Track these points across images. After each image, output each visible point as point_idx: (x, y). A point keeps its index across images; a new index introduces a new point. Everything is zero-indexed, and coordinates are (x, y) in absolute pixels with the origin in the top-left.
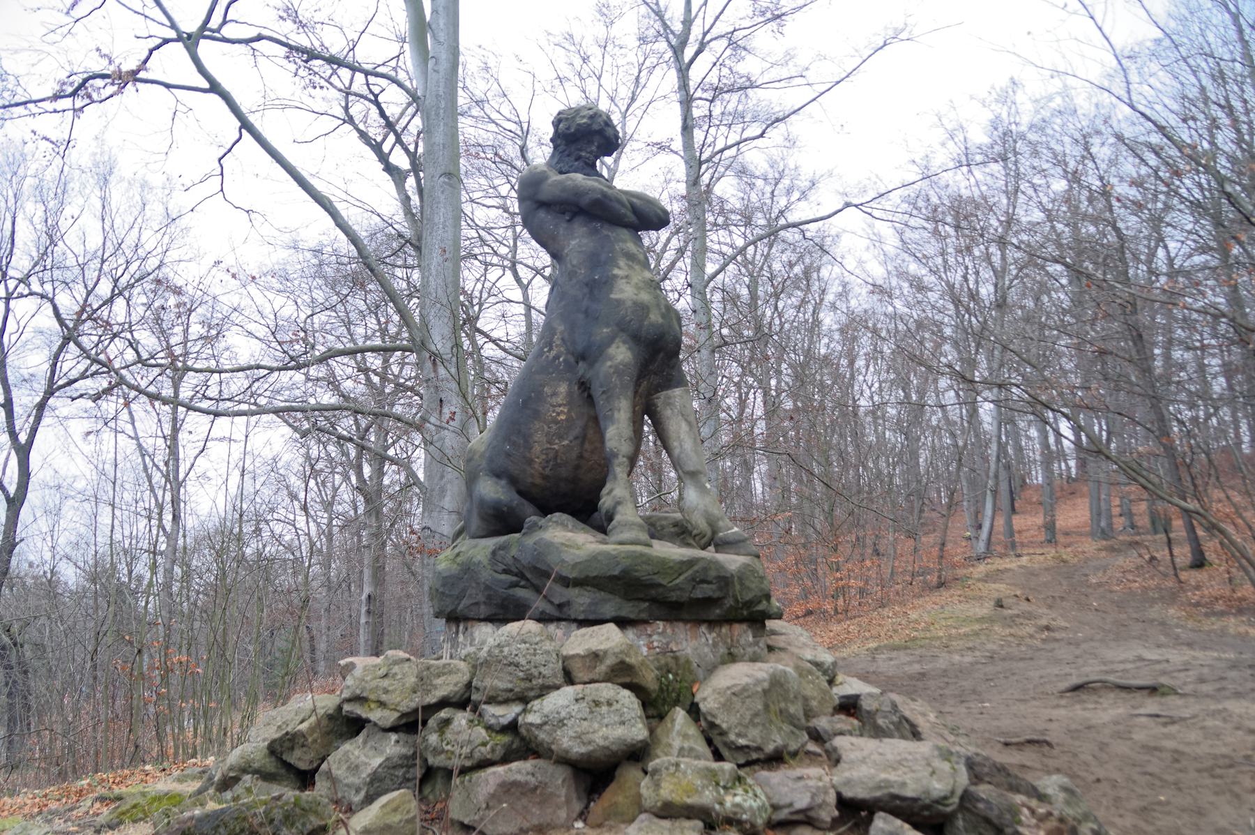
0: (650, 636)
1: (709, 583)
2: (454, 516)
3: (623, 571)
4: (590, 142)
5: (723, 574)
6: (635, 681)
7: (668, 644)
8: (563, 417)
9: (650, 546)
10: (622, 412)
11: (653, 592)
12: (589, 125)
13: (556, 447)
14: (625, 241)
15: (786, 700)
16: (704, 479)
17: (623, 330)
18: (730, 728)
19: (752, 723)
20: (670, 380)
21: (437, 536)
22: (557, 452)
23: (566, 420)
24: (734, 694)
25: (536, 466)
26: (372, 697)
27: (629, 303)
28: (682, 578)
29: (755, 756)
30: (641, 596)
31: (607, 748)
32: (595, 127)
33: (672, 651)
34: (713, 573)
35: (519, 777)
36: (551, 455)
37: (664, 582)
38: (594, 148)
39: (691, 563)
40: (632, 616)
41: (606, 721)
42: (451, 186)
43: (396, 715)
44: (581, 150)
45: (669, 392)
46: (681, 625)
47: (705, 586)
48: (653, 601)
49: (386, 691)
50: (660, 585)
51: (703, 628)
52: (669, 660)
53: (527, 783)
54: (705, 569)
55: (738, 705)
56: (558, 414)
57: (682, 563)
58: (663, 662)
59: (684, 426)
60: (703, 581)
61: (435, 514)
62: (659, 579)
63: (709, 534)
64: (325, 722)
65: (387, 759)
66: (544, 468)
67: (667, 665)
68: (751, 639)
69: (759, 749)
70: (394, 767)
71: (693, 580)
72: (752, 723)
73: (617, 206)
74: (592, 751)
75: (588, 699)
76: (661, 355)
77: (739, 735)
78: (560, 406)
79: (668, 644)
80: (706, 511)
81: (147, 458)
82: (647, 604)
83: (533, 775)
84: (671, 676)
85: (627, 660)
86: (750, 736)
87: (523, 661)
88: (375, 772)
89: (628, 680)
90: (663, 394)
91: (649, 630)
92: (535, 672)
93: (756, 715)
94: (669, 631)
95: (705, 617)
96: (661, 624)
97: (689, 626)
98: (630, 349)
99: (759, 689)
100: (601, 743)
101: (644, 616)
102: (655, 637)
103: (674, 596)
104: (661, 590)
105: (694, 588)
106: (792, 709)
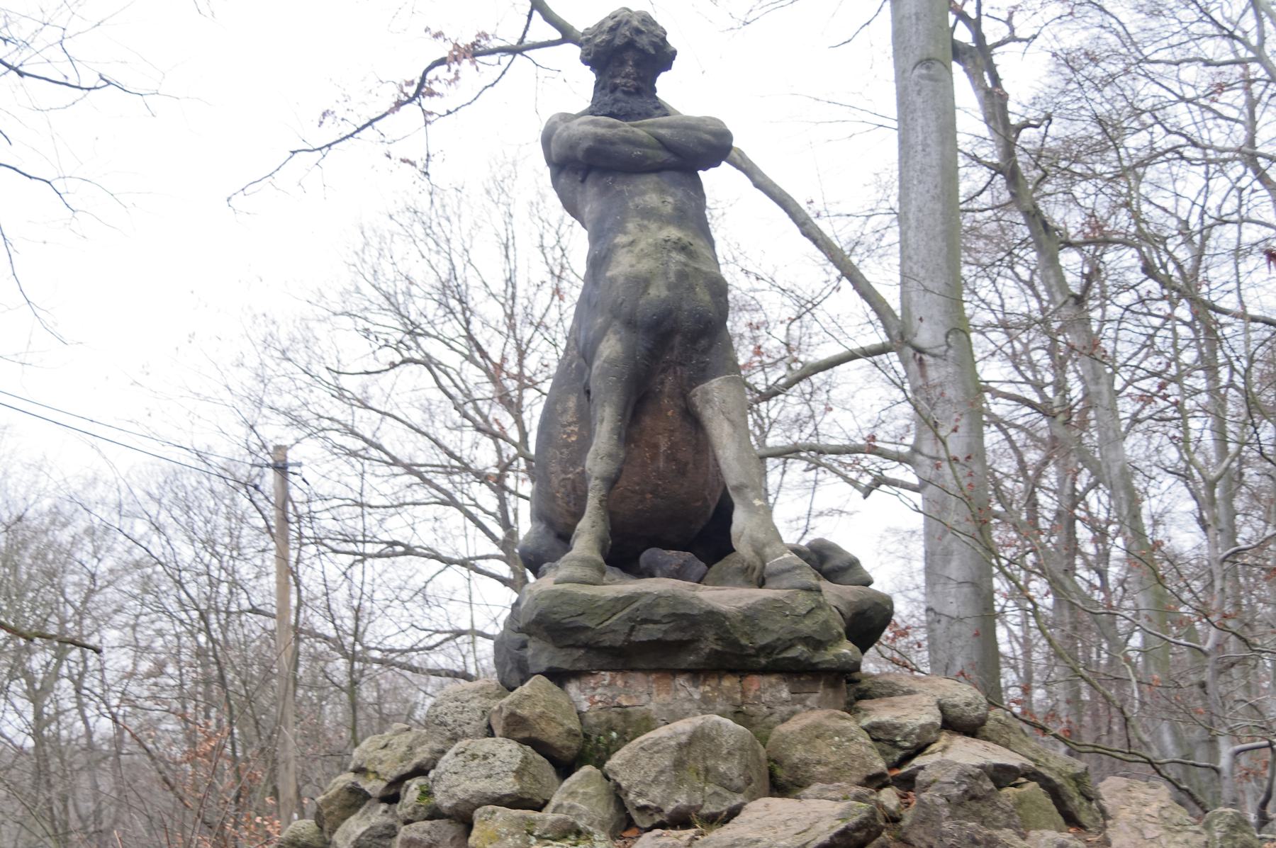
0: (594, 689)
1: (656, 622)
2: (966, 589)
3: (539, 615)
4: (623, 63)
5: (682, 610)
6: (533, 735)
7: (613, 698)
8: (574, 438)
9: (819, 591)
10: (605, 424)
11: (582, 637)
12: (609, 42)
13: (570, 476)
14: (643, 193)
15: (716, 755)
16: (751, 495)
17: (615, 317)
18: (630, 787)
19: (655, 781)
20: (704, 370)
21: (944, 620)
22: (573, 481)
23: (577, 442)
24: (642, 748)
25: (560, 502)
26: (370, 768)
27: (621, 280)
28: (615, 618)
29: (658, 818)
30: (571, 642)
31: (467, 801)
32: (618, 41)
33: (620, 706)
34: (663, 611)
35: (416, 835)
36: (569, 487)
37: (591, 624)
38: (629, 69)
39: (630, 599)
40: (566, 666)
41: (472, 774)
42: (931, 78)
43: (384, 784)
44: (614, 77)
45: (706, 385)
46: (639, 676)
47: (650, 626)
48: (587, 646)
49: (381, 762)
50: (587, 628)
51: (681, 681)
52: (614, 715)
53: (421, 841)
54: (649, 607)
55: (644, 762)
56: (569, 436)
57: (617, 600)
58: (603, 719)
59: (727, 428)
60: (645, 621)
61: (939, 588)
62: (582, 621)
63: (758, 564)
64: (345, 795)
65: (372, 828)
66: (568, 503)
67: (609, 721)
68: (785, 694)
69: (659, 810)
70: (380, 837)
71: (630, 619)
72: (655, 781)
73: (626, 148)
74: (456, 805)
75: (469, 752)
76: (678, 339)
77: (640, 794)
78: (570, 424)
79: (613, 698)
80: (751, 537)
81: (327, 542)
82: (582, 651)
83: (429, 833)
84: (614, 734)
85: (518, 711)
86: (651, 796)
87: (449, 720)
88: (358, 840)
89: (526, 734)
90: (698, 390)
91: (592, 682)
92: (459, 732)
93: (662, 772)
94: (620, 683)
95: (671, 665)
96: (607, 677)
97: (654, 676)
98: (620, 340)
99: (673, 743)
100: (462, 795)
101: (581, 665)
102: (599, 690)
103: (607, 640)
104: (590, 634)
105: (632, 629)
106: (722, 768)
